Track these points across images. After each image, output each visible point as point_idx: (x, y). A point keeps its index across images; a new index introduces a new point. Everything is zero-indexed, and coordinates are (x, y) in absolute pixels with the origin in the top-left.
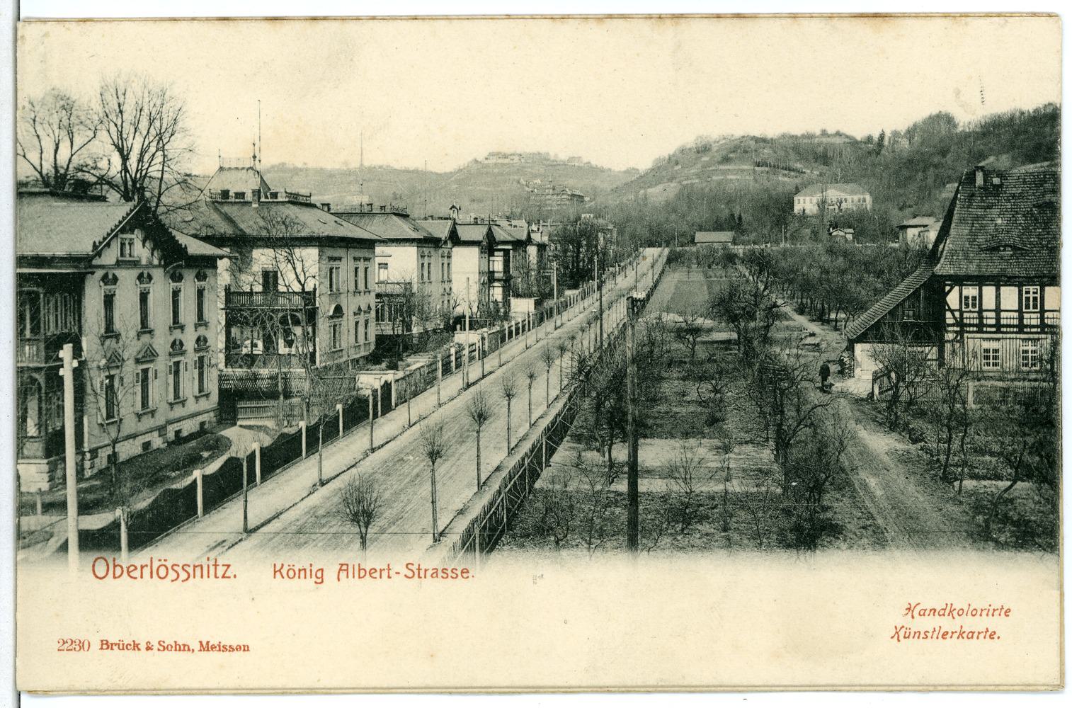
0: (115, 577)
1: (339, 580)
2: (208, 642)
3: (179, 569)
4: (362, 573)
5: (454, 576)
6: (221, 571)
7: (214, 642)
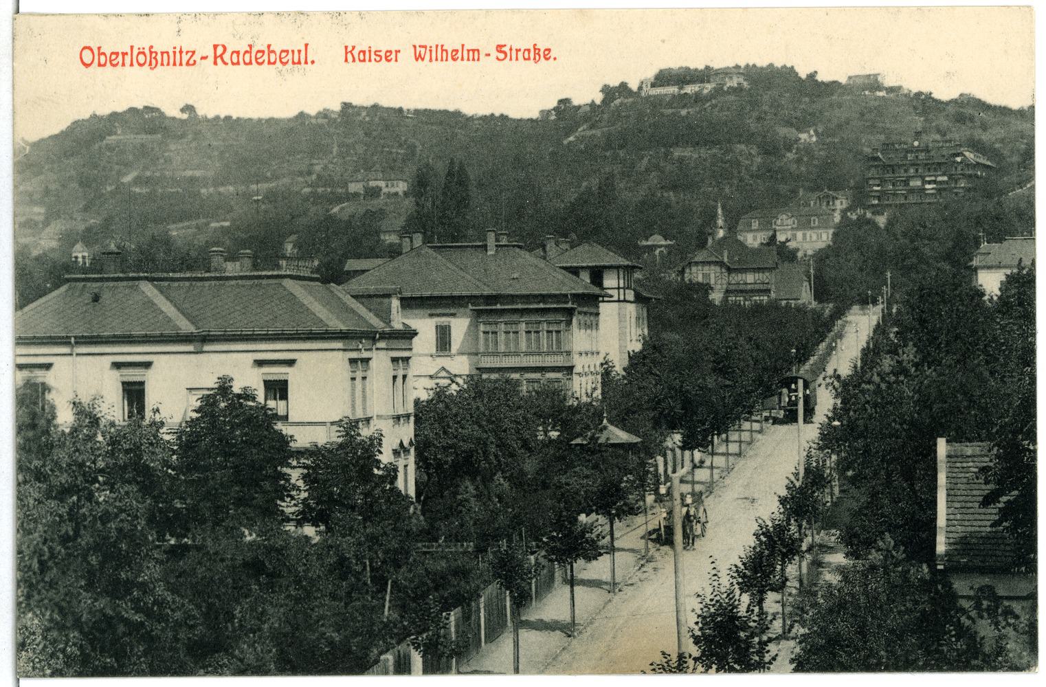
5: (378, 58)
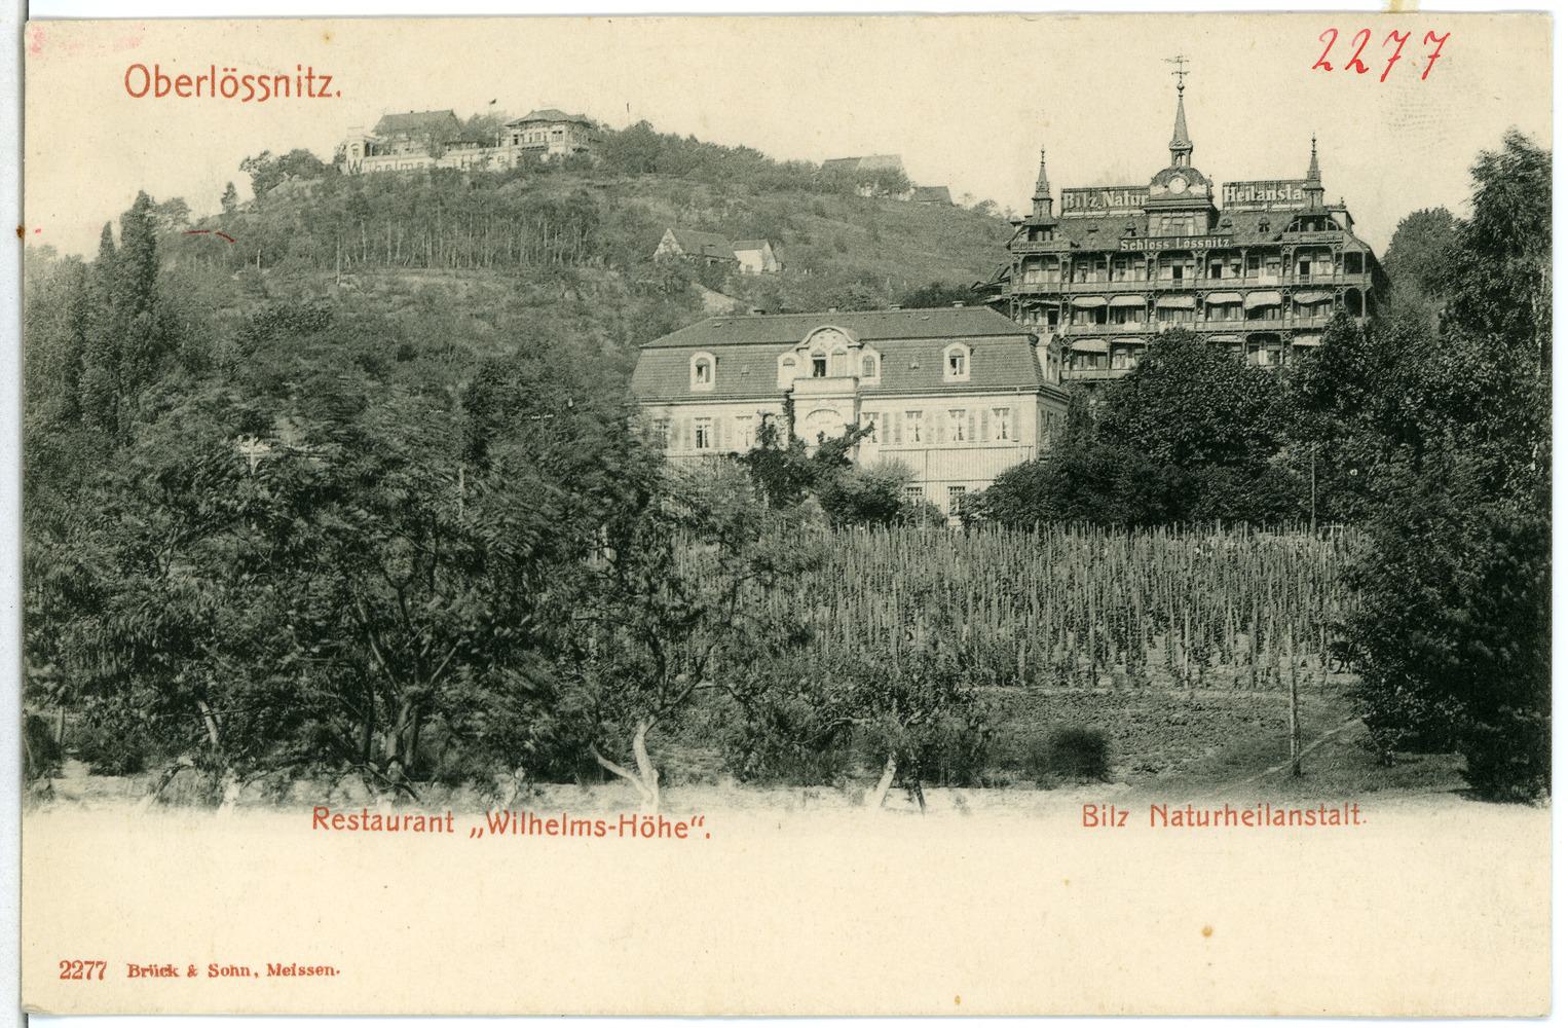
0: (158, 95)
2: (279, 966)
3: (254, 84)
6: (317, 85)
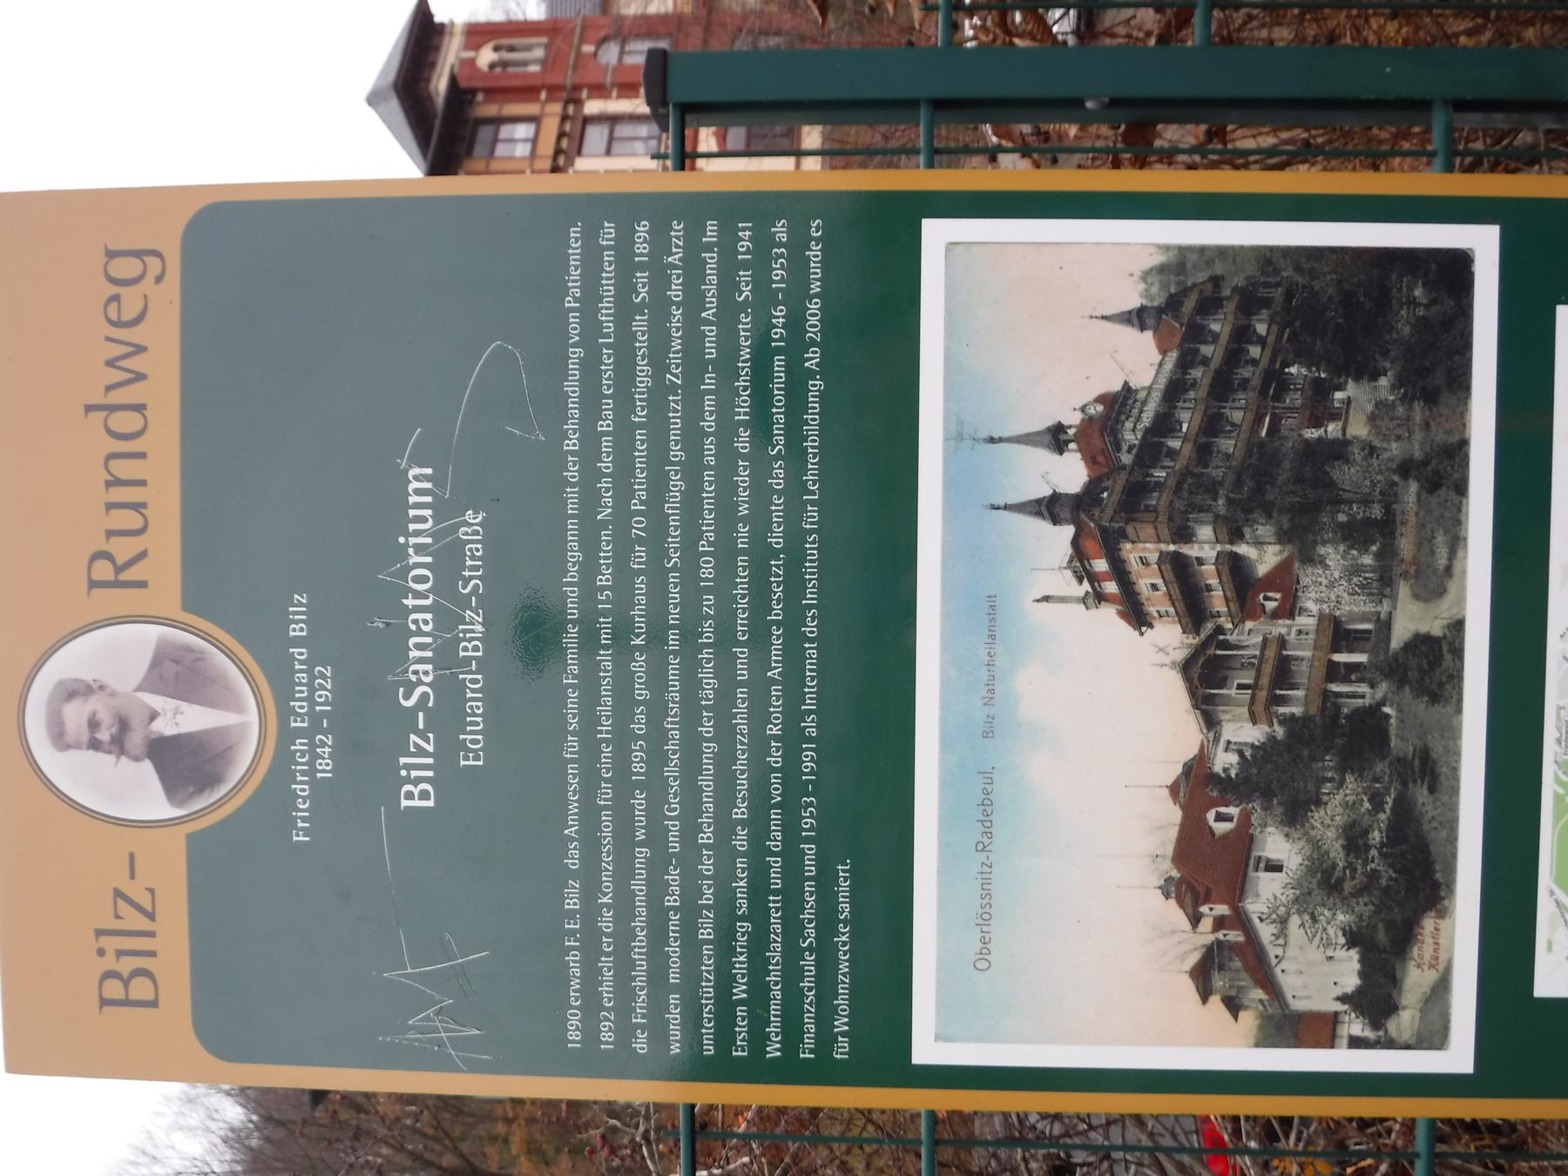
1: (145, 296)
4: (987, 802)
7: (996, 436)
